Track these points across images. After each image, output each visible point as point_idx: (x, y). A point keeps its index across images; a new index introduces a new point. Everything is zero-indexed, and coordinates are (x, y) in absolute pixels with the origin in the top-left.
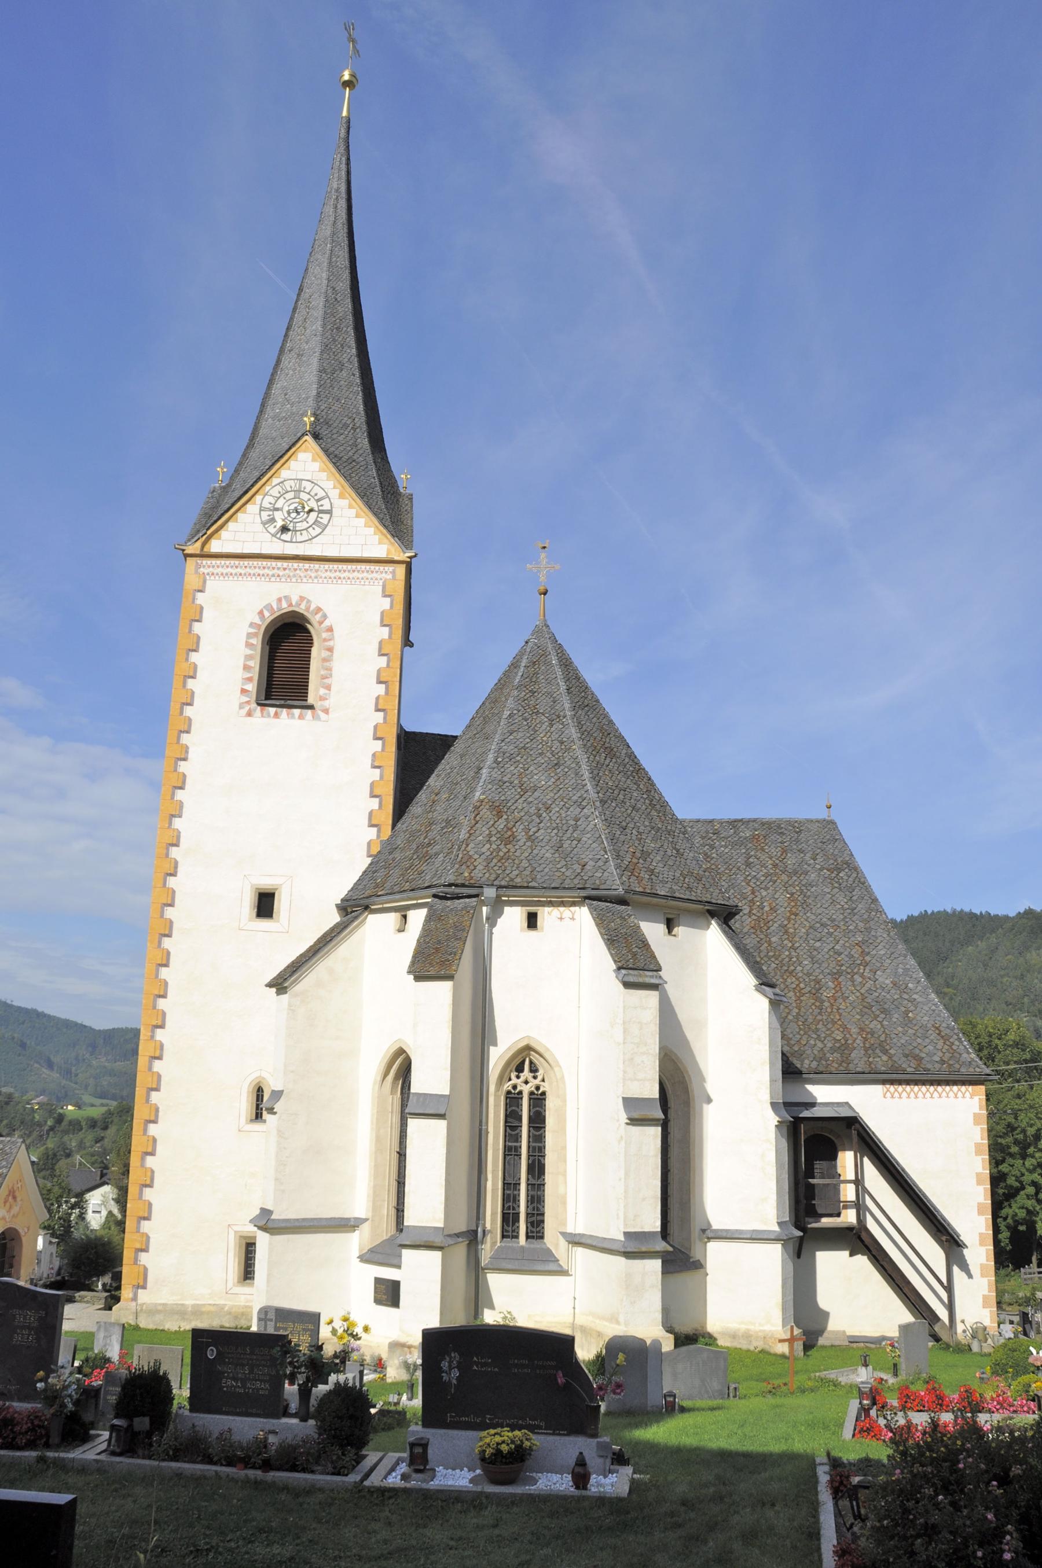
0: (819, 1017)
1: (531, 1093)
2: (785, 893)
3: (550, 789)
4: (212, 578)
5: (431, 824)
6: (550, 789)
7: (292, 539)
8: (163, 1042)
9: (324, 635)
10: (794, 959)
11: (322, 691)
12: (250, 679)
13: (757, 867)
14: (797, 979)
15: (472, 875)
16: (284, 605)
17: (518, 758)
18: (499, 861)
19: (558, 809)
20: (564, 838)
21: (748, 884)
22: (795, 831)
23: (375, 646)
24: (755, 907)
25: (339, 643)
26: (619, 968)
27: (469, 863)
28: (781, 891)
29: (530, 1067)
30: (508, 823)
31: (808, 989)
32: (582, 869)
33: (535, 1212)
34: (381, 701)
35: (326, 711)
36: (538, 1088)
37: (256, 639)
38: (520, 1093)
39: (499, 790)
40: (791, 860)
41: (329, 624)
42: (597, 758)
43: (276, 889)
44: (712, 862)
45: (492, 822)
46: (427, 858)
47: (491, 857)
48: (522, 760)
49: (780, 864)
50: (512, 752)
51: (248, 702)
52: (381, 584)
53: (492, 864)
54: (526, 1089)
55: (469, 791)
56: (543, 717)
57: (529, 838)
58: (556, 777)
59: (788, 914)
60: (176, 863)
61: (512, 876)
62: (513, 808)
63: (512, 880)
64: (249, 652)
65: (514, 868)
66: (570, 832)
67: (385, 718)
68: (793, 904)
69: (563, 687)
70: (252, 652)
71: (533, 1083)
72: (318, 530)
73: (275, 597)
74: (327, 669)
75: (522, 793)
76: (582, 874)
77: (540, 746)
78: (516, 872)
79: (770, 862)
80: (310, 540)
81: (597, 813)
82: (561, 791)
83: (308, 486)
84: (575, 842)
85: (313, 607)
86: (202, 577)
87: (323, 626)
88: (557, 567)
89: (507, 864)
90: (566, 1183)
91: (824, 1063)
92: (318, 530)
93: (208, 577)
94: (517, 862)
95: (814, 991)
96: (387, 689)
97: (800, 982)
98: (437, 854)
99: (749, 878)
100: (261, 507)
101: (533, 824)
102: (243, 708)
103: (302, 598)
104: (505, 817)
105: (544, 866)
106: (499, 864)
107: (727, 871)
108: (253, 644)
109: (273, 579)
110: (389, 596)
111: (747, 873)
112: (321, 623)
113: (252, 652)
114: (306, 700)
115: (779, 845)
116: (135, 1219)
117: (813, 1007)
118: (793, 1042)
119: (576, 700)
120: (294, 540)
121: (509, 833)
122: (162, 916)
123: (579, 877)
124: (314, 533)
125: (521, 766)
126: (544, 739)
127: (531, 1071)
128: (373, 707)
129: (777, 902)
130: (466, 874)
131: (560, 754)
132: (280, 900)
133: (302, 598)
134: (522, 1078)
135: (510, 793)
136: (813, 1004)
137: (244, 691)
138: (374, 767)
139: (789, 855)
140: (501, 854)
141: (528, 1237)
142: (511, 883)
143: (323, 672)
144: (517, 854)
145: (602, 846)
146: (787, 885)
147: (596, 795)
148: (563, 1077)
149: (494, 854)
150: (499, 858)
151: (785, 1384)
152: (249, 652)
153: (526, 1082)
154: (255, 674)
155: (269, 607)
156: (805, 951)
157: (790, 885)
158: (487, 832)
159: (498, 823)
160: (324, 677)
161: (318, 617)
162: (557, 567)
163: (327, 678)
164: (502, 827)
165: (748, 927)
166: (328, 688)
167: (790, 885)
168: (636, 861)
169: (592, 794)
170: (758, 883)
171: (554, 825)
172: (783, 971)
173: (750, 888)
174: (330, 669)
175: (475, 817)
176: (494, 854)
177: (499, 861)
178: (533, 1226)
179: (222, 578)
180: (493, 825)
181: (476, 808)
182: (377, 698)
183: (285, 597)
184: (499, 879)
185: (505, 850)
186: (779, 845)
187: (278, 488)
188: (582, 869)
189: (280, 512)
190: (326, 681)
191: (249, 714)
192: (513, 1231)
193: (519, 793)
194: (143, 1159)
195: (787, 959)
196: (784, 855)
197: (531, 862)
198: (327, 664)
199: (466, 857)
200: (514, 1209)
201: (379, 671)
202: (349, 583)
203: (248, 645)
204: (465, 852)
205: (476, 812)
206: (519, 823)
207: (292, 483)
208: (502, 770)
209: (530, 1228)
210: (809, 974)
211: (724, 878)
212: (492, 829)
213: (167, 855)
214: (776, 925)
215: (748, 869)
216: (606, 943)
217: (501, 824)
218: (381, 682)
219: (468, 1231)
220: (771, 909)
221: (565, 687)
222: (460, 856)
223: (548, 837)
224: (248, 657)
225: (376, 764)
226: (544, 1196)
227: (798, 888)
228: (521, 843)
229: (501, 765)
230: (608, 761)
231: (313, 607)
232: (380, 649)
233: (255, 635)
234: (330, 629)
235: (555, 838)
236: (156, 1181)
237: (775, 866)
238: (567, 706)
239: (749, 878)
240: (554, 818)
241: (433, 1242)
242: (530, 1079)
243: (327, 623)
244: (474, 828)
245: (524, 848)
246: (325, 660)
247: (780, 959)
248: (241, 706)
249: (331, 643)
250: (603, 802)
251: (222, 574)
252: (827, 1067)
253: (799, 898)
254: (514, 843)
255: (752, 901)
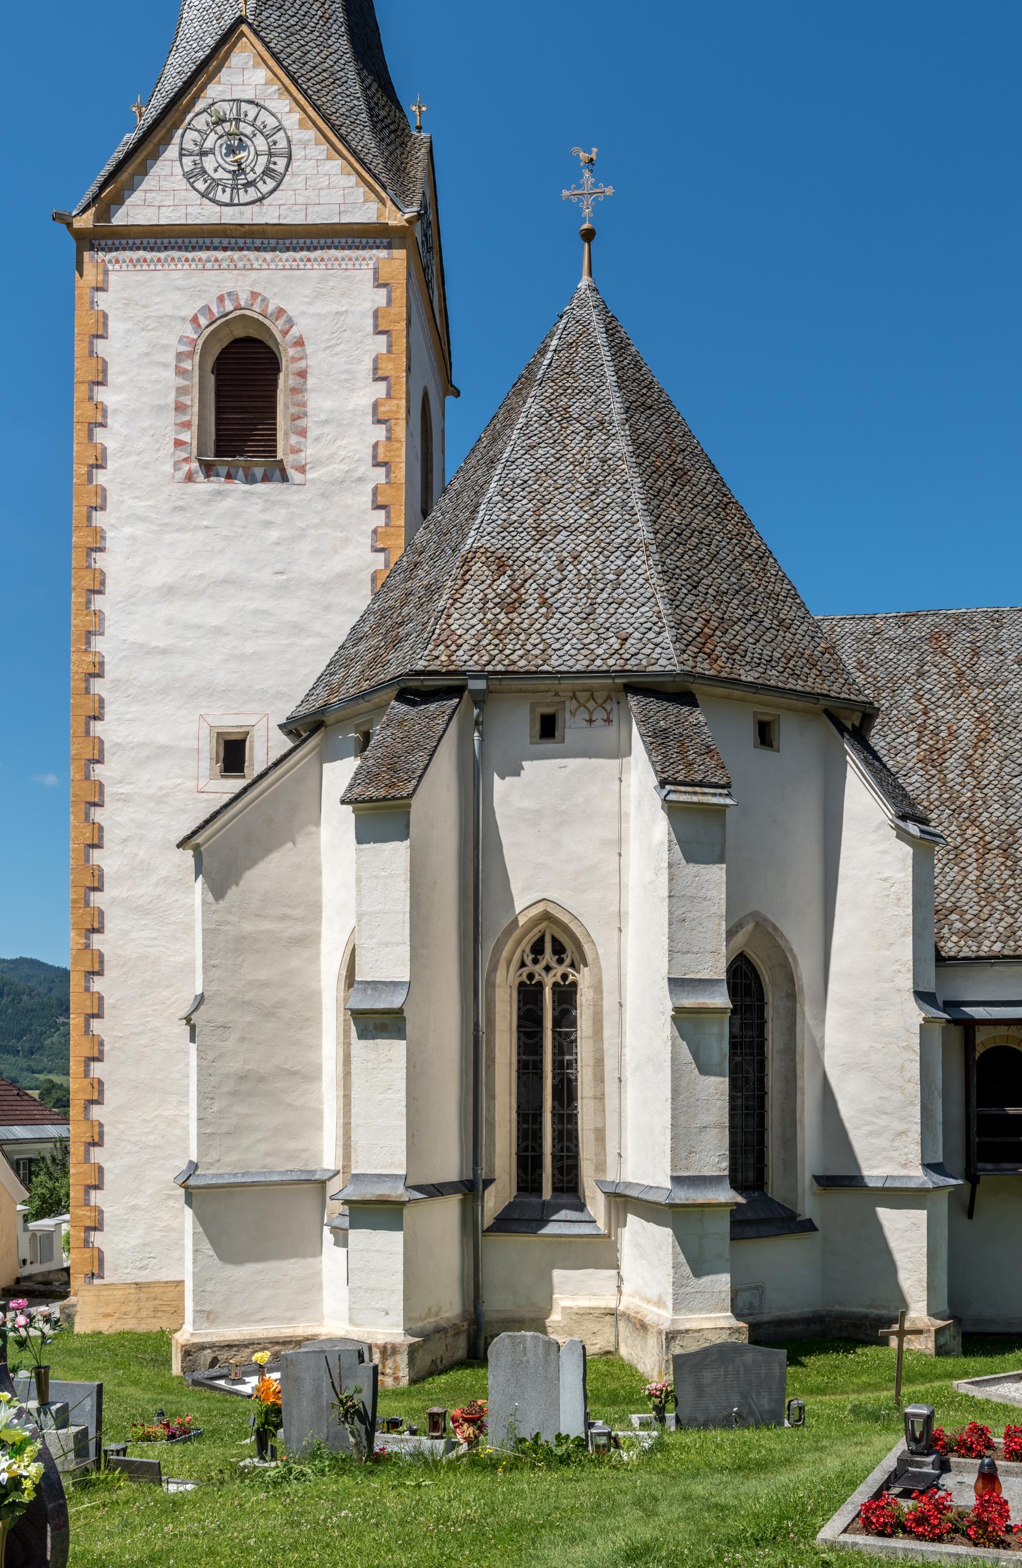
0: (1011, 882)
1: (556, 985)
2: (972, 712)
3: (581, 529)
4: (117, 267)
5: (407, 595)
6: (581, 529)
7: (231, 199)
8: (103, 951)
9: (291, 352)
10: (980, 802)
11: (294, 439)
12: (187, 425)
13: (935, 677)
14: (982, 830)
15: (453, 658)
16: (229, 306)
17: (536, 487)
18: (496, 636)
19: (590, 558)
20: (599, 600)
21: (918, 701)
22: (993, 626)
23: (368, 364)
24: (927, 732)
25: (316, 360)
26: (663, 783)
27: (449, 642)
28: (967, 709)
29: (553, 946)
30: (514, 581)
31: (996, 843)
32: (622, 645)
33: (565, 1154)
34: (381, 450)
35: (302, 469)
36: (565, 977)
37: (190, 361)
38: (540, 985)
39: (503, 534)
40: (985, 666)
41: (298, 334)
42: (660, 483)
43: (247, 733)
44: (869, 673)
45: (488, 582)
46: (396, 643)
47: (485, 631)
48: (542, 489)
49: (968, 671)
50: (526, 478)
51: (186, 460)
52: (371, 266)
53: (485, 642)
54: (549, 981)
55: (459, 540)
56: (578, 425)
57: (544, 602)
58: (591, 512)
59: (975, 741)
60: (102, 701)
61: (514, 657)
62: (523, 558)
63: (514, 663)
64: (181, 382)
65: (518, 647)
66: (608, 590)
67: (387, 476)
68: (983, 726)
69: (611, 379)
70: (186, 383)
71: (560, 970)
72: (271, 184)
73: (215, 293)
74: (299, 405)
75: (537, 537)
76: (621, 652)
77: (571, 467)
78: (521, 652)
79: (954, 669)
80: (260, 200)
81: (651, 562)
82: (598, 533)
83: (252, 111)
84: (615, 606)
85: (271, 308)
86: (101, 266)
87: (288, 337)
88: (609, 191)
89: (507, 641)
90: (604, 1111)
91: (1012, 943)
92: (271, 184)
93: (110, 267)
94: (522, 637)
95: (1005, 846)
96: (389, 430)
97: (986, 834)
98: (408, 635)
99: (921, 693)
100: (182, 149)
101: (553, 581)
102: (179, 469)
103: (254, 295)
104: (509, 573)
105: (565, 641)
106: (496, 641)
107: (889, 685)
108: (186, 371)
109: (209, 265)
110: (385, 285)
111: (919, 687)
112: (285, 333)
113: (186, 383)
114: (275, 457)
115: (968, 645)
116: (82, 1189)
117: (1003, 868)
118: (968, 917)
119: (632, 398)
120: (236, 201)
121: (514, 596)
122: (87, 778)
123: (617, 656)
124: (265, 189)
125: (539, 497)
126: (579, 456)
127: (555, 952)
128: (369, 460)
129: (960, 724)
130: (443, 658)
131: (600, 478)
132: (252, 749)
133: (254, 295)
134: (543, 964)
135: (523, 540)
136: (1002, 863)
137: (178, 444)
138: (376, 550)
139: (983, 659)
140: (500, 626)
141: (555, 1189)
142: (511, 668)
143: (293, 410)
144: (524, 626)
145: (656, 609)
146: (976, 701)
147: (652, 536)
148: (598, 958)
149: (490, 627)
150: (496, 632)
151: (135, 1425)
152: (181, 382)
153: (548, 969)
154: (193, 415)
155: (206, 309)
156: (996, 790)
157: (981, 701)
158: (481, 596)
159: (498, 582)
160: (296, 418)
161: (280, 323)
162: (609, 191)
163: (299, 418)
164: (504, 586)
165: (914, 761)
166: (303, 433)
167: (981, 701)
168: (710, 632)
169: (645, 534)
170: (933, 700)
171: (584, 582)
172: (961, 819)
173: (921, 707)
174: (304, 405)
175: (463, 575)
176: (490, 627)
177: (496, 636)
178: (562, 1174)
179: (131, 268)
180: (490, 586)
181: (466, 561)
182: (375, 446)
183: (229, 294)
184: (493, 663)
185: (506, 621)
186: (968, 645)
187: (205, 117)
188: (622, 645)
189: (211, 156)
190: (299, 422)
191: (189, 478)
192: (533, 1181)
193: (533, 537)
194: (86, 1109)
195: (969, 803)
196: (975, 659)
197: (545, 637)
198: (299, 397)
199: (447, 632)
200: (533, 1150)
201: (375, 406)
202: (323, 267)
203: (180, 372)
204: (445, 626)
205: (465, 568)
206: (530, 581)
207: (226, 106)
208: (510, 505)
209: (558, 1176)
210: (999, 823)
211: (884, 695)
212: (489, 591)
213: (87, 690)
214: (955, 756)
215: (920, 681)
216: (646, 748)
217: (503, 584)
218: (379, 422)
219: (461, 1182)
220: (950, 734)
221: (615, 379)
222: (437, 631)
223: (573, 600)
224: (181, 391)
225: (380, 545)
226: (577, 1130)
227: (991, 704)
228: (531, 610)
229: (509, 497)
230: (675, 489)
231: (271, 308)
232: (375, 369)
233: (190, 355)
234: (300, 342)
235: (584, 600)
236: (106, 1138)
237: (961, 674)
238: (617, 407)
239: (921, 693)
240: (584, 571)
241: (389, 1196)
242: (553, 964)
243: (295, 332)
244: (462, 591)
245: (536, 616)
246: (294, 391)
247: (958, 803)
248: (177, 466)
249: (302, 364)
250: (662, 548)
251: (131, 261)
252: (1016, 950)
253: (993, 718)
254: (521, 610)
255: (923, 726)
